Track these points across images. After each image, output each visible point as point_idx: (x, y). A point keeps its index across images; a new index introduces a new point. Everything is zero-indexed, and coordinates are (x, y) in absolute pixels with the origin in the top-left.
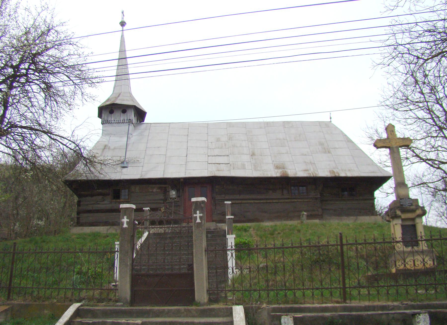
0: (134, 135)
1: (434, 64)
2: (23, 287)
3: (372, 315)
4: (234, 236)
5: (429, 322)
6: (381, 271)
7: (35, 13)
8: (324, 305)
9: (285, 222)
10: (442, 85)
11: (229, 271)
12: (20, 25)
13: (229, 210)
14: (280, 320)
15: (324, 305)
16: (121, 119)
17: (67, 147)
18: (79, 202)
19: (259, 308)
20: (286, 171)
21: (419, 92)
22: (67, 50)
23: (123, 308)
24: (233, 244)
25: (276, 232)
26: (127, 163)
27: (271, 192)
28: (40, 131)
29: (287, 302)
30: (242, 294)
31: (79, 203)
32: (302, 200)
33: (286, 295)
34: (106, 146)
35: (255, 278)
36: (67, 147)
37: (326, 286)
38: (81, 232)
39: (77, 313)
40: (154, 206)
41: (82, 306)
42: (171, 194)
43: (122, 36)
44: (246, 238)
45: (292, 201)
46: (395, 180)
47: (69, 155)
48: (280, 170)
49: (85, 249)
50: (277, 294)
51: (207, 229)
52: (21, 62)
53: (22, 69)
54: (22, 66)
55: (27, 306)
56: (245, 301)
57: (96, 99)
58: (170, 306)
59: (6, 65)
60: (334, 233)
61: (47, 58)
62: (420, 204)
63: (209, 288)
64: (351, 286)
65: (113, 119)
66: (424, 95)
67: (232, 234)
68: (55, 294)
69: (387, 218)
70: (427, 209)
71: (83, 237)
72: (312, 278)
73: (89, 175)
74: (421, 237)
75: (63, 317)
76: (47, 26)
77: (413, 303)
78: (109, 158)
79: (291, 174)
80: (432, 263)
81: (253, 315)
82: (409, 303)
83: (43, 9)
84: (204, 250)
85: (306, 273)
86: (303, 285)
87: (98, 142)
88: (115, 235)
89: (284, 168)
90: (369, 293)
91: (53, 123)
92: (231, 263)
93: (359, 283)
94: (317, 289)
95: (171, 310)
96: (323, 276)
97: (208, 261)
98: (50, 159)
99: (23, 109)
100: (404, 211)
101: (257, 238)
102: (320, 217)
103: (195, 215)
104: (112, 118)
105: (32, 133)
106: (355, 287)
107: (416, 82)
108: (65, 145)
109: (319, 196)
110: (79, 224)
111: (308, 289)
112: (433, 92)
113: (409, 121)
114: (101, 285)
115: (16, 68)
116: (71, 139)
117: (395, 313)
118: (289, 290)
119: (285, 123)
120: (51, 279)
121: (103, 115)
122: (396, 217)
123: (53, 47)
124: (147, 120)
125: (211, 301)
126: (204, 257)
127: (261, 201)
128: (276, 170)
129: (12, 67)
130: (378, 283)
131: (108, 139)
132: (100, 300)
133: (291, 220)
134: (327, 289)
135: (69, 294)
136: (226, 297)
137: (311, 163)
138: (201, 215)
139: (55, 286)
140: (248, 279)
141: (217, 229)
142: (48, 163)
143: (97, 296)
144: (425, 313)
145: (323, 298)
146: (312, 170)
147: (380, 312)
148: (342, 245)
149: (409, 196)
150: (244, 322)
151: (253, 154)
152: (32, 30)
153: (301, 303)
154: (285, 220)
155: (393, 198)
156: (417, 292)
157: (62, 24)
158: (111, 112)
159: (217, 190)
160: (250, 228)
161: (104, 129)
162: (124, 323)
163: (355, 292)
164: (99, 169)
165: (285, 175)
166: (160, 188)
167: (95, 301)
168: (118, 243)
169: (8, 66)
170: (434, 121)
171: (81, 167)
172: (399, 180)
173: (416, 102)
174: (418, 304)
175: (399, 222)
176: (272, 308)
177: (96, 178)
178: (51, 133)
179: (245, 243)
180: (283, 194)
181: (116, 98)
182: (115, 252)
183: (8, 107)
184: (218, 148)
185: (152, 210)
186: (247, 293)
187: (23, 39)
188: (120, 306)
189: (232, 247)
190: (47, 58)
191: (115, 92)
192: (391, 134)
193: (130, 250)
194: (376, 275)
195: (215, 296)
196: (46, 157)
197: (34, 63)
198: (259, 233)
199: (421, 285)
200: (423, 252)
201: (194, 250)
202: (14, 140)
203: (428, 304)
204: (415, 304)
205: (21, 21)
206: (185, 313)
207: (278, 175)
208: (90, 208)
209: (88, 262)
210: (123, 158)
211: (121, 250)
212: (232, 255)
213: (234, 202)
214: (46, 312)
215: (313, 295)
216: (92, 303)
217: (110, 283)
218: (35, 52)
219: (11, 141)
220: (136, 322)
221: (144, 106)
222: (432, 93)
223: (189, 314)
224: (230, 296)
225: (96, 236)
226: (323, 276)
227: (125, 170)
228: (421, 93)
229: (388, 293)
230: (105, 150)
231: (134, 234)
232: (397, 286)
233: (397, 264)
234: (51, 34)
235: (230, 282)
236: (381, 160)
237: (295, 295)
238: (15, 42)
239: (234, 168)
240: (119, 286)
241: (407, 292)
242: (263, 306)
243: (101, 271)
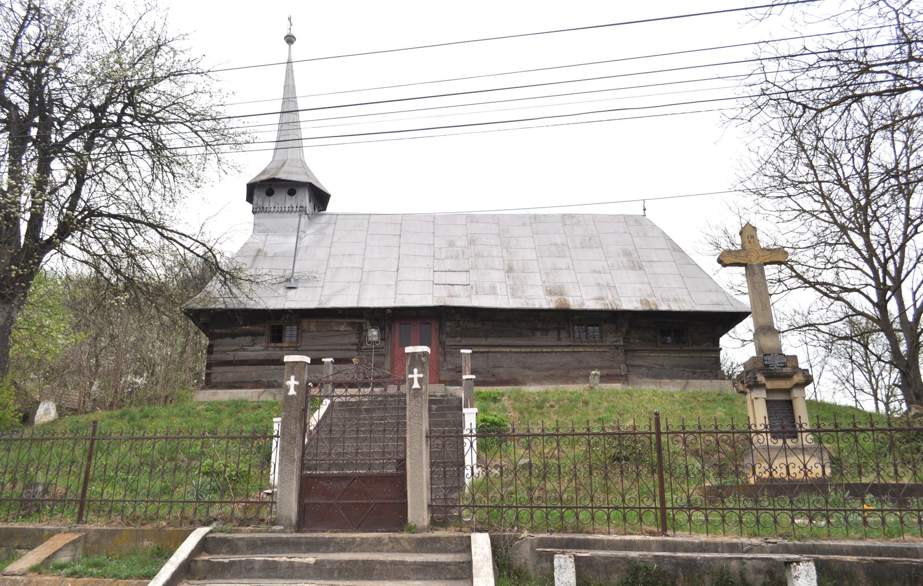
0: (309, 232)
2: (107, 500)
3: (713, 559)
4: (475, 410)
5: (815, 577)
6: (729, 480)
8: (628, 537)
9: (561, 386)
12: (106, 34)
13: (467, 365)
14: (552, 561)
15: (628, 537)
16: (287, 206)
17: (192, 251)
19: (516, 539)
21: (807, 165)
23: (284, 536)
24: (474, 426)
25: (548, 405)
26: (296, 280)
27: (539, 334)
29: (563, 529)
30: (488, 513)
31: (210, 350)
33: (562, 518)
35: (510, 484)
36: (192, 251)
38: (215, 398)
39: (204, 545)
40: (340, 355)
41: (211, 532)
44: (495, 413)
46: (756, 322)
47: (193, 263)
49: (221, 431)
51: (430, 396)
52: (109, 101)
53: (111, 114)
54: (111, 109)
55: (113, 533)
56: (493, 526)
57: (243, 171)
58: (364, 531)
59: (81, 105)
61: (155, 96)
62: (803, 365)
64: (676, 505)
65: (272, 206)
67: (472, 406)
68: (164, 511)
69: (741, 388)
70: (815, 373)
71: (216, 408)
72: (608, 488)
73: (229, 300)
75: (177, 553)
76: (156, 39)
77: (786, 542)
78: (265, 271)
79: (574, 303)
80: (820, 470)
82: (780, 541)
84: (424, 435)
85: (597, 478)
86: (592, 500)
87: (246, 244)
89: (562, 295)
90: (707, 520)
91: (166, 210)
92: (470, 458)
93: (689, 501)
94: (616, 508)
95: (367, 539)
96: (627, 484)
97: (431, 452)
98: (161, 272)
99: (111, 185)
100: (770, 376)
101: (514, 415)
103: (410, 376)
105: (129, 226)
108: (188, 249)
110: (210, 384)
111: (600, 508)
112: (831, 164)
113: (785, 216)
114: (247, 496)
115: (100, 111)
116: (199, 239)
117: (752, 559)
118: (568, 508)
120: (158, 484)
121: (255, 198)
122: (755, 385)
123: (165, 77)
124: (331, 207)
125: (435, 523)
126: (424, 447)
127: (523, 350)
128: (548, 298)
129: (92, 108)
130: (723, 502)
132: (244, 522)
134: (633, 508)
135: (189, 511)
136: (460, 517)
137: (608, 285)
138: (421, 375)
139: (165, 497)
140: (498, 486)
141: (447, 396)
142: (156, 279)
143: (238, 514)
144: (809, 561)
145: (625, 524)
146: (610, 298)
147: (727, 555)
148: (659, 434)
150: (491, 563)
151: (510, 270)
152: (129, 46)
153: (588, 533)
155: (751, 351)
156: (793, 522)
157: (184, 37)
158: (270, 193)
159: (448, 329)
160: (503, 395)
162: (286, 562)
163: (682, 517)
164: (246, 290)
165: (563, 307)
166: (349, 324)
167: (235, 523)
168: (279, 419)
169: (84, 106)
170: (833, 217)
171: (215, 287)
172: (763, 322)
174: (795, 545)
175: (762, 394)
176: (537, 539)
177: (242, 307)
178: (163, 228)
179: (493, 423)
180: (559, 339)
182: (272, 437)
183: (84, 180)
184: (452, 257)
185: (337, 361)
187: (112, 60)
189: (471, 431)
190: (155, 96)
191: (276, 158)
192: (749, 242)
193: (298, 435)
194: (718, 487)
195: (441, 515)
196: (154, 269)
198: (517, 405)
199: (800, 509)
200: (804, 450)
201: (408, 436)
202: (95, 237)
203: (814, 545)
205: (109, 29)
206: (390, 545)
207: (552, 306)
208: (230, 357)
209: (226, 452)
210: (288, 273)
211: (283, 434)
212: (471, 446)
213: (476, 350)
214: (146, 543)
215: (609, 518)
217: (261, 489)
219: (90, 239)
220: (306, 560)
221: (325, 184)
223: (396, 547)
224: (468, 516)
225: (238, 405)
226: (627, 484)
227: (292, 292)
229: (741, 521)
230: (259, 258)
231: (306, 406)
232: (757, 510)
233: (757, 470)
234: (163, 54)
235: (467, 491)
236: (730, 288)
237: (577, 518)
238: (96, 65)
241: (775, 521)
242: (523, 536)
243: (246, 469)
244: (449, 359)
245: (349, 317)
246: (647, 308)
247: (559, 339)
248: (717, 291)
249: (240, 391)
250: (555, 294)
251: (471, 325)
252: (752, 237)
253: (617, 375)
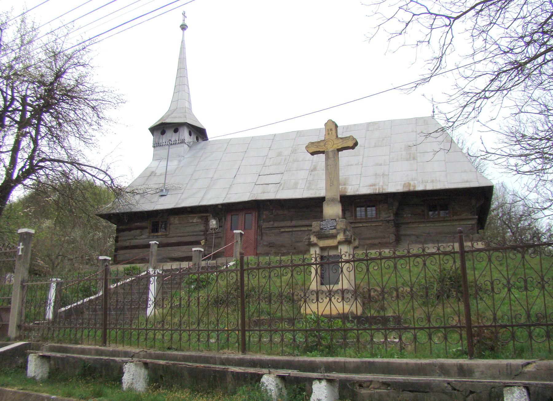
20: (345, 188)
32: (369, 225)
34: (153, 172)
43: (183, 42)
45: (356, 226)
104: (164, 140)
109: (392, 218)
158: (163, 133)
166: (201, 217)
178: (79, 164)
184: (276, 165)
208: (127, 244)
221: (203, 122)
244: (265, 238)
245: (201, 212)
246: (406, 190)
251: (280, 212)
253: (386, 243)
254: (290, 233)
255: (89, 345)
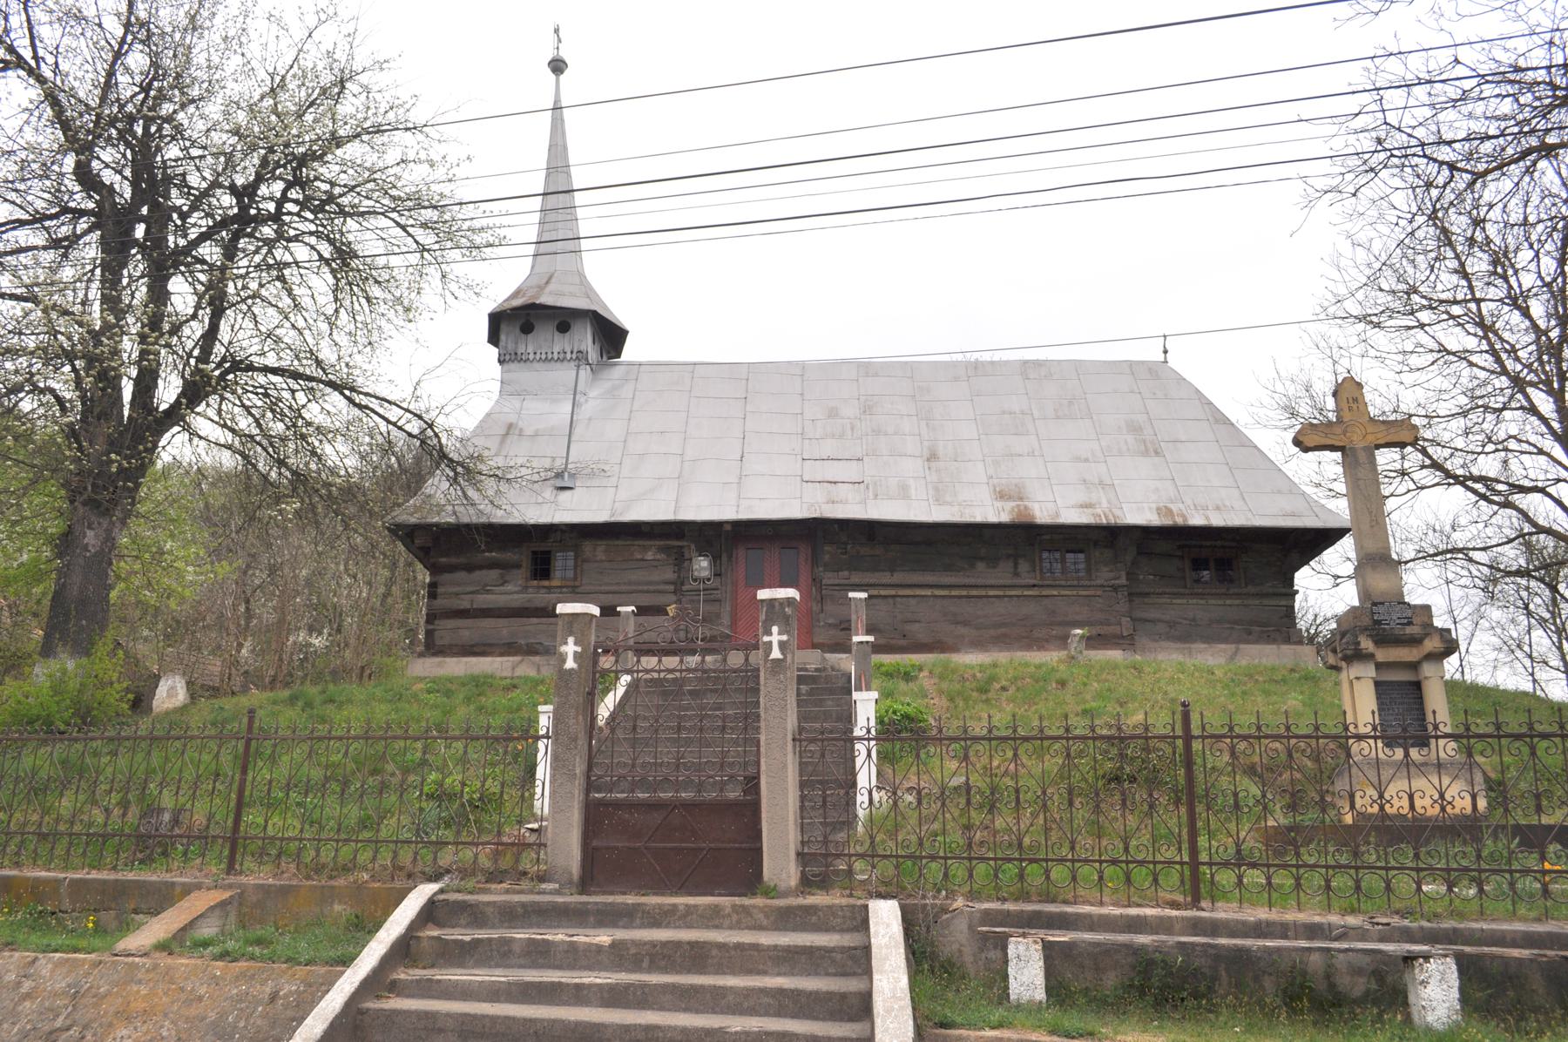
1: (1507, 185)
2: (273, 838)
3: (1278, 949)
4: (875, 695)
6: (1309, 817)
7: (299, 33)
8: (1133, 911)
9: (1019, 654)
10: (1531, 246)
11: (859, 799)
13: (859, 618)
14: (1005, 948)
15: (1133, 911)
16: (556, 349)
17: (400, 428)
18: (433, 586)
19: (945, 910)
22: (400, 144)
23: (560, 899)
24: (873, 723)
25: (997, 686)
26: (572, 476)
27: (981, 566)
28: (322, 382)
29: (1024, 896)
30: (897, 867)
33: (1021, 876)
36: (400, 428)
37: (1140, 857)
38: (441, 672)
39: (430, 913)
40: (646, 600)
41: (441, 891)
42: (696, 567)
46: (1359, 547)
48: (1009, 505)
50: (996, 871)
51: (799, 670)
55: (285, 891)
56: (904, 888)
60: (1166, 693)
63: (803, 843)
64: (1216, 859)
65: (530, 350)
66: (1469, 281)
67: (868, 689)
68: (364, 857)
71: (444, 688)
74: (1436, 727)
75: (387, 925)
77: (1406, 923)
78: (520, 461)
81: (928, 931)
82: (1396, 921)
83: (323, 17)
84: (790, 737)
85: (1082, 813)
88: (536, 683)
89: (1021, 499)
90: (1269, 883)
92: (866, 776)
96: (1132, 821)
98: (352, 462)
100: (1384, 639)
102: (1125, 641)
104: (529, 345)
105: (297, 387)
106: (1226, 864)
107: (1446, 237)
108: (394, 424)
109: (1123, 581)
110: (433, 648)
114: (499, 834)
116: (411, 408)
119: (1030, 369)
120: (353, 813)
121: (503, 337)
122: (1357, 656)
125: (808, 883)
126: (790, 756)
127: (954, 593)
128: (999, 504)
129: (233, 189)
130: (1298, 854)
131: (518, 405)
132: (494, 876)
133: (1041, 648)
134: (1142, 863)
135: (406, 856)
138: (785, 638)
139: (366, 835)
141: (825, 669)
144: (1446, 956)
146: (1105, 504)
148: (1188, 738)
149: (1402, 595)
150: (902, 950)
151: (932, 457)
153: (1065, 902)
154: (1021, 648)
155: (1348, 597)
156: (1419, 889)
157: (381, 65)
158: (527, 329)
161: (508, 376)
163: (1226, 878)
164: (490, 493)
165: (1023, 520)
166: (661, 549)
171: (438, 486)
172: (1372, 546)
173: (1442, 302)
174: (1422, 928)
175: (1369, 671)
176: (980, 911)
177: (483, 520)
178: (352, 389)
180: (1016, 574)
181: (541, 288)
182: (538, 738)
184: (833, 436)
185: (642, 611)
186: (909, 863)
188: (551, 893)
189: (869, 731)
191: (537, 270)
192: (1350, 409)
194: (1290, 829)
195: (818, 869)
196: (341, 456)
197: (297, 182)
198: (944, 685)
203: (1455, 930)
204: (1415, 925)
206: (735, 917)
207: (1005, 518)
209: (463, 761)
210: (559, 463)
212: (869, 755)
213: (875, 592)
214: (337, 908)
215: (1101, 878)
216: (471, 884)
218: (302, 150)
220: (597, 940)
221: (620, 313)
222: (1495, 273)
223: (744, 919)
224: (862, 872)
225: (480, 684)
226: (1132, 821)
228: (1462, 272)
229: (1328, 887)
234: (350, 97)
236: (1316, 487)
237: (1048, 877)
239: (876, 496)
240: (549, 835)
241: (1388, 888)
244: (829, 607)
246: (1167, 522)
247: (1016, 574)
248: (1291, 492)
249: (482, 659)
250: (1010, 498)
252: (1355, 400)
254: (891, 601)
255: (49, 870)
